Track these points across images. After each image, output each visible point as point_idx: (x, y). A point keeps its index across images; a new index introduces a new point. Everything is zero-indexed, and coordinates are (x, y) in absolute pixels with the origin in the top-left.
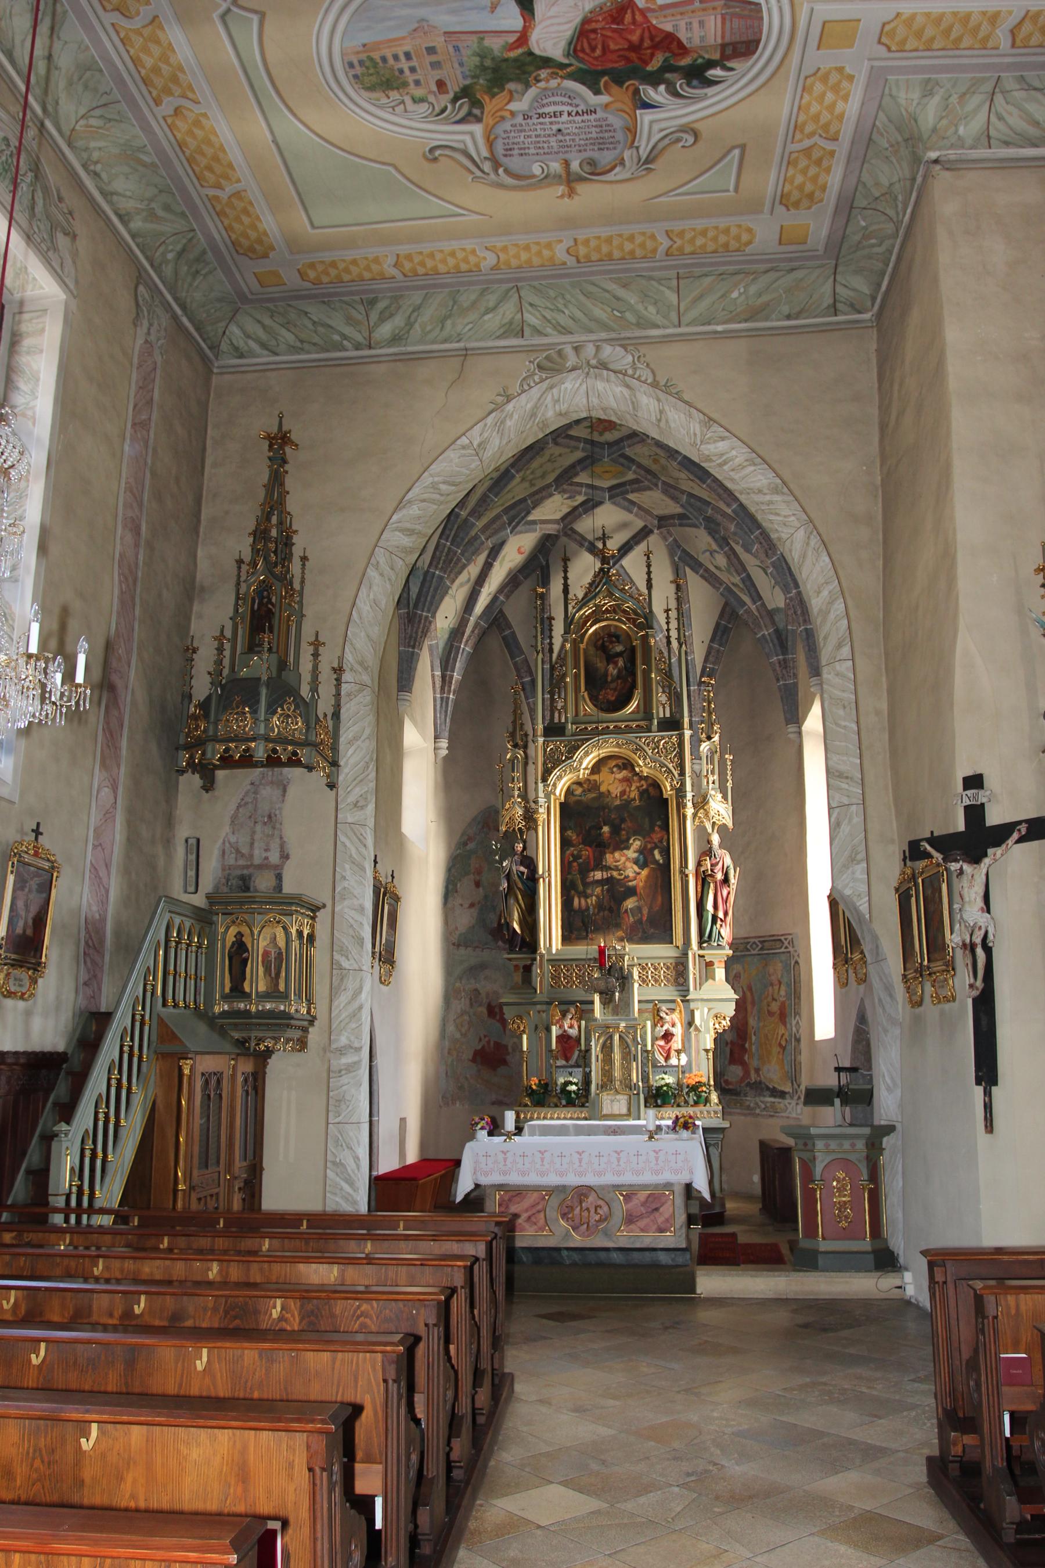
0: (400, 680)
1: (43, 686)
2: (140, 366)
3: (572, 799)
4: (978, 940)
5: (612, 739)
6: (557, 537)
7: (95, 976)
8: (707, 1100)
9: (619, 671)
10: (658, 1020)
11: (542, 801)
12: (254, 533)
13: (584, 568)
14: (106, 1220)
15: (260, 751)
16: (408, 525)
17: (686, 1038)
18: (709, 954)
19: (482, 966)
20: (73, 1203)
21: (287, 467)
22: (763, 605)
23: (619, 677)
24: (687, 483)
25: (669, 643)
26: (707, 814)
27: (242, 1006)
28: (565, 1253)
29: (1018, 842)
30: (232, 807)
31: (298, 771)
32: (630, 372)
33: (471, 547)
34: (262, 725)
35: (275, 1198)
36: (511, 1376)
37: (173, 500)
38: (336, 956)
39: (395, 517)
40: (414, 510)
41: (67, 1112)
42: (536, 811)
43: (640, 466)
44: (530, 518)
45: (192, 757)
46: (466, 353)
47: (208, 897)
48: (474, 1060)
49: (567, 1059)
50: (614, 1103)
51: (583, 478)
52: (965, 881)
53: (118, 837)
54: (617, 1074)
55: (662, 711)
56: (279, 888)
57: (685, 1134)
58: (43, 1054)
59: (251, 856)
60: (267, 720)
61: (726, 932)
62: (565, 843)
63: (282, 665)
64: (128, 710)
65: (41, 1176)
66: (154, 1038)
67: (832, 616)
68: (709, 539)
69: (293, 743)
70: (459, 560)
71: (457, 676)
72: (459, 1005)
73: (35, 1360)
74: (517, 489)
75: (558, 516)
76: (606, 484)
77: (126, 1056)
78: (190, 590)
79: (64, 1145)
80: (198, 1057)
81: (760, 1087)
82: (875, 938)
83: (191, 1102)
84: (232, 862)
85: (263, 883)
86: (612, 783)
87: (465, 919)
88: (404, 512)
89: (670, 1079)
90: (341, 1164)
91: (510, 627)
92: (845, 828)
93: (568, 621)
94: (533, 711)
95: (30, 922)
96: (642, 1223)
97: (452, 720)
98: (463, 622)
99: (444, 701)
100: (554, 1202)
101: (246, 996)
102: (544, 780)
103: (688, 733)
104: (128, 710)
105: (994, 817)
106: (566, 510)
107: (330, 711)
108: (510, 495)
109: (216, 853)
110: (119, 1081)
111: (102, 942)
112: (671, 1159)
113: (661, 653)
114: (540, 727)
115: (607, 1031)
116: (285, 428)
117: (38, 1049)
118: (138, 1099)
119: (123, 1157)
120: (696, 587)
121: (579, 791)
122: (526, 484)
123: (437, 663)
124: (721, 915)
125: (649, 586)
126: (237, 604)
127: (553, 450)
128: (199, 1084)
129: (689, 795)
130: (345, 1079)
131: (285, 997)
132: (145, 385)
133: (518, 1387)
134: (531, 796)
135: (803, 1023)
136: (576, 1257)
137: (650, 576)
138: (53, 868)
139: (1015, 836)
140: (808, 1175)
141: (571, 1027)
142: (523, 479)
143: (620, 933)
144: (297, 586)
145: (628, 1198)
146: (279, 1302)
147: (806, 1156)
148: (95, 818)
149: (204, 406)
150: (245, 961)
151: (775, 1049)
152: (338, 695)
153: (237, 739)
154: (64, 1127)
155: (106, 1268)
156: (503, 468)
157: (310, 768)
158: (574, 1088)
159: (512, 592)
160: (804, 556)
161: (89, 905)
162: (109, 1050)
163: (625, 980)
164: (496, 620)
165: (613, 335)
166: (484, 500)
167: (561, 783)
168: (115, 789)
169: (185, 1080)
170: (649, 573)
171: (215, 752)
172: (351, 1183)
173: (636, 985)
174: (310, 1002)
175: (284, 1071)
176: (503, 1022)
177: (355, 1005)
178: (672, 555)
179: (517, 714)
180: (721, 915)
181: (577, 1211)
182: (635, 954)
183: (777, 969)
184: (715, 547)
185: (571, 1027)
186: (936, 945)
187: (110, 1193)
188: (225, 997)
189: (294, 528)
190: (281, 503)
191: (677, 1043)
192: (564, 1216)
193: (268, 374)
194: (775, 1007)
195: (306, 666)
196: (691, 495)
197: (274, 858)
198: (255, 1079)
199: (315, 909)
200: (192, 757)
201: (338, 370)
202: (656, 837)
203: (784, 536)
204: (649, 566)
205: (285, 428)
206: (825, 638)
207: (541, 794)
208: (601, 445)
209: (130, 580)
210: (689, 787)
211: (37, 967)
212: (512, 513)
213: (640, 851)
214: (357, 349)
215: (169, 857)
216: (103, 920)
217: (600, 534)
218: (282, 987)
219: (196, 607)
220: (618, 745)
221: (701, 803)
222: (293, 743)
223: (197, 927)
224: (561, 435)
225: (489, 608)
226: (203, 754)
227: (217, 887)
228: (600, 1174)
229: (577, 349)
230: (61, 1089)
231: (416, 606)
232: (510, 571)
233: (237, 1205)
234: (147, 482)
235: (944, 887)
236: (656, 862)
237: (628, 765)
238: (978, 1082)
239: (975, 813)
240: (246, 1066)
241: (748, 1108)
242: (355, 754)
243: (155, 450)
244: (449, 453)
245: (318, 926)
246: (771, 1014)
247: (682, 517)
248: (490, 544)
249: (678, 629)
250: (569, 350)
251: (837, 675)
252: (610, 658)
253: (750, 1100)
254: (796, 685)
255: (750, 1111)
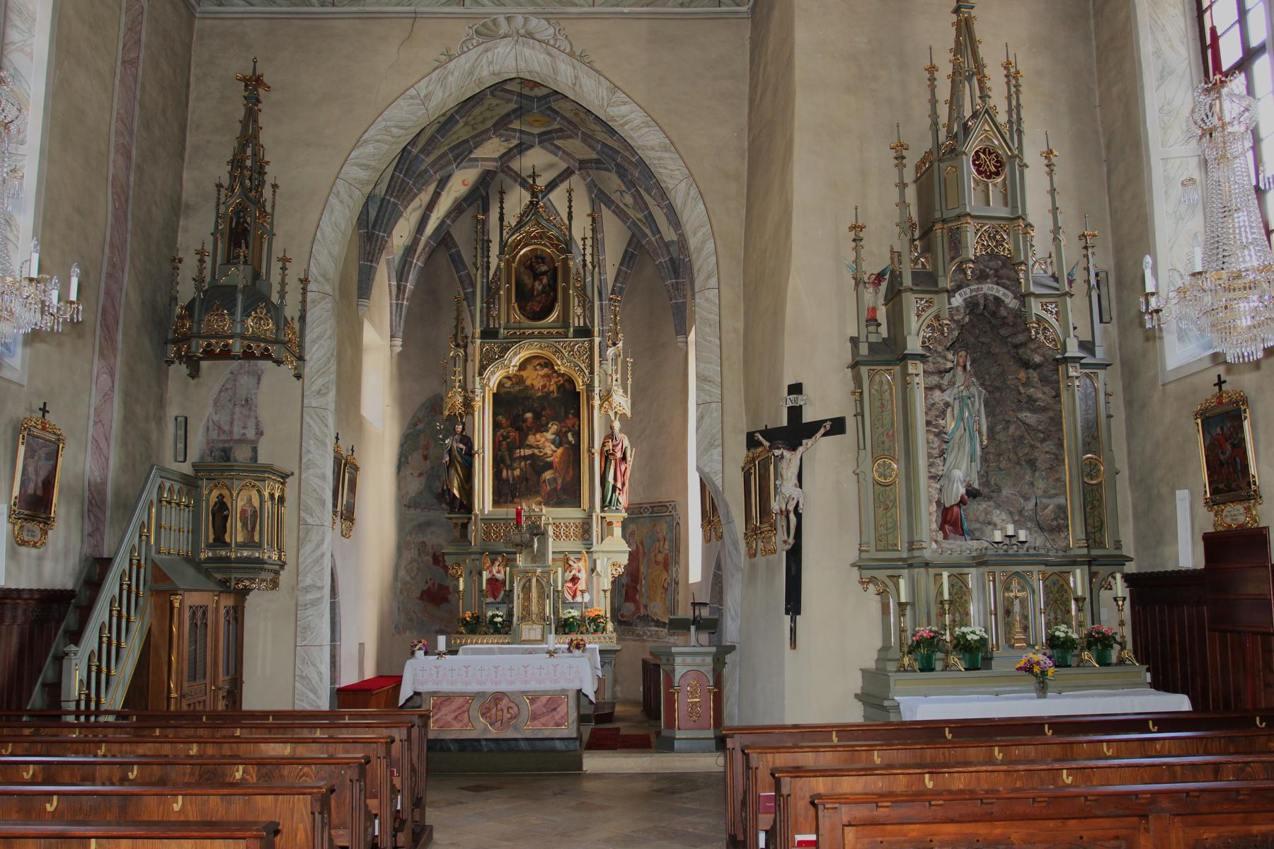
0: (360, 288)
1: (43, 302)
2: (128, 10)
3: (503, 390)
4: (791, 508)
5: (536, 342)
6: (495, 173)
7: (98, 529)
8: (604, 629)
9: (544, 287)
10: (567, 567)
11: (478, 391)
12: (232, 162)
13: (517, 200)
14: (111, 719)
15: (237, 346)
16: (365, 161)
17: (589, 582)
18: (609, 516)
19: (428, 524)
20: (83, 707)
21: (260, 106)
22: (661, 237)
23: (543, 292)
24: (601, 136)
25: (585, 265)
26: (611, 405)
27: (223, 553)
28: (484, 743)
29: (824, 435)
30: (217, 388)
31: (269, 364)
32: (552, 42)
33: (421, 179)
34: (239, 326)
35: (251, 701)
36: (431, 827)
37: (160, 125)
38: (303, 514)
39: (353, 154)
40: (370, 149)
41: (76, 637)
42: (473, 400)
43: (564, 118)
44: (473, 156)
45: (179, 350)
46: (415, 16)
47: (194, 465)
48: (421, 598)
49: (495, 597)
50: (531, 631)
51: (516, 125)
52: (784, 464)
53: (115, 415)
54: (534, 608)
55: (577, 321)
56: (255, 458)
57: (577, 652)
58: (54, 591)
59: (231, 432)
60: (243, 321)
61: (623, 499)
62: (496, 425)
63: (256, 275)
64: (122, 308)
65: (54, 689)
66: (149, 578)
67: (704, 253)
68: (619, 181)
69: (264, 340)
70: (411, 189)
71: (410, 286)
72: (409, 555)
73: (49, 808)
74: (461, 132)
75: (496, 155)
76: (536, 131)
77: (125, 593)
78: (176, 208)
79: (74, 662)
80: (187, 594)
81: (647, 620)
82: (727, 506)
83: (182, 628)
84: (215, 437)
85: (242, 454)
86: (534, 378)
87: (415, 486)
88: (361, 150)
89: (575, 613)
90: (307, 677)
91: (456, 246)
92: (707, 420)
93: (503, 245)
94: (473, 316)
95: (40, 484)
96: (543, 720)
97: (406, 322)
98: (415, 242)
99: (399, 306)
100: (476, 705)
101: (228, 545)
102: (481, 374)
103: (597, 340)
104: (122, 308)
105: (808, 416)
106: (503, 151)
107: (297, 315)
108: (455, 137)
109: (201, 430)
110: (120, 612)
111: (104, 501)
112: (577, 672)
113: (578, 273)
114: (478, 331)
115: (527, 575)
116: (258, 73)
117: (49, 587)
118: (136, 626)
119: (125, 671)
120: (610, 221)
121: (508, 384)
122: (469, 128)
123: (394, 274)
124: (619, 485)
125: (570, 217)
126: (217, 222)
127: (490, 100)
128: (187, 615)
129: (597, 390)
130: (309, 612)
131: (259, 546)
132: (133, 27)
133: (436, 836)
134: (470, 387)
135: (681, 570)
136: (492, 745)
137: (572, 208)
138: (59, 440)
139: (822, 431)
140: (670, 683)
141: (499, 572)
142: (466, 124)
143: (539, 499)
144: (268, 209)
145: (533, 701)
146: (241, 767)
147: (668, 668)
148: (95, 399)
149: (189, 48)
150: (226, 518)
151: (660, 590)
152: (304, 302)
153: (217, 336)
154: (73, 648)
155: (108, 750)
156: (448, 114)
157: (279, 362)
158: (499, 619)
159: (457, 217)
160: (685, 204)
161: (92, 471)
162: (111, 587)
163: (542, 534)
164: (444, 239)
165: (539, 10)
166: (432, 139)
167: (495, 377)
168: (112, 375)
169: (176, 611)
170: (570, 207)
171: (199, 346)
172: (315, 692)
173: (551, 540)
174: (280, 550)
175: (259, 605)
176: (446, 568)
177: (319, 553)
178: (590, 191)
179: (459, 319)
180: (619, 485)
181: (493, 711)
182: (550, 515)
183: (663, 528)
184: (623, 188)
185: (499, 572)
186: (765, 511)
187: (115, 699)
188: (209, 546)
189: (266, 159)
190: (255, 137)
191: (582, 585)
192: (483, 715)
193: (245, 22)
194: (660, 558)
195: (275, 278)
196: (604, 145)
197: (251, 434)
198: (236, 612)
199: (285, 476)
200: (179, 350)
201: (307, 22)
202: (570, 422)
203: (671, 186)
204: (570, 201)
205: (258, 73)
206: (699, 271)
207: (478, 386)
208: (531, 99)
209: (123, 198)
210: (596, 383)
211: (47, 521)
212: (456, 152)
213: (557, 434)
214: (322, 5)
215: (161, 432)
216: (104, 483)
217: (530, 172)
218: (257, 539)
219: (182, 223)
220: (541, 348)
221: (606, 397)
222: (264, 340)
223: (185, 490)
224: (499, 88)
225: (438, 229)
226: (189, 347)
227: (202, 457)
228: (511, 683)
229: (508, 19)
230: (71, 619)
231: (374, 227)
232: (456, 199)
233: (221, 706)
234: (137, 113)
235: (772, 467)
236: (569, 443)
237: (548, 364)
238: (787, 613)
239: (795, 412)
240: (227, 601)
241: (638, 635)
242: (319, 349)
243: (143, 88)
244: (400, 102)
245: (287, 490)
246: (657, 563)
247: (597, 161)
248: (438, 176)
249: (592, 255)
250: (501, 19)
251: (706, 300)
252: (537, 276)
253: (639, 629)
254: (684, 303)
255: (640, 638)
